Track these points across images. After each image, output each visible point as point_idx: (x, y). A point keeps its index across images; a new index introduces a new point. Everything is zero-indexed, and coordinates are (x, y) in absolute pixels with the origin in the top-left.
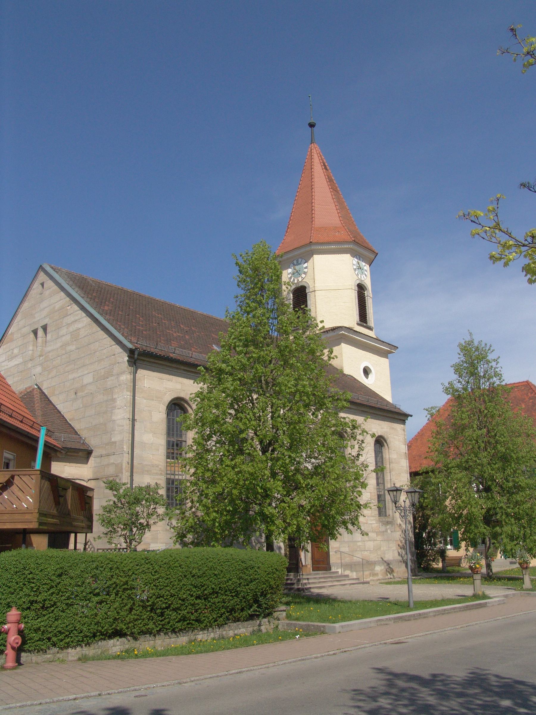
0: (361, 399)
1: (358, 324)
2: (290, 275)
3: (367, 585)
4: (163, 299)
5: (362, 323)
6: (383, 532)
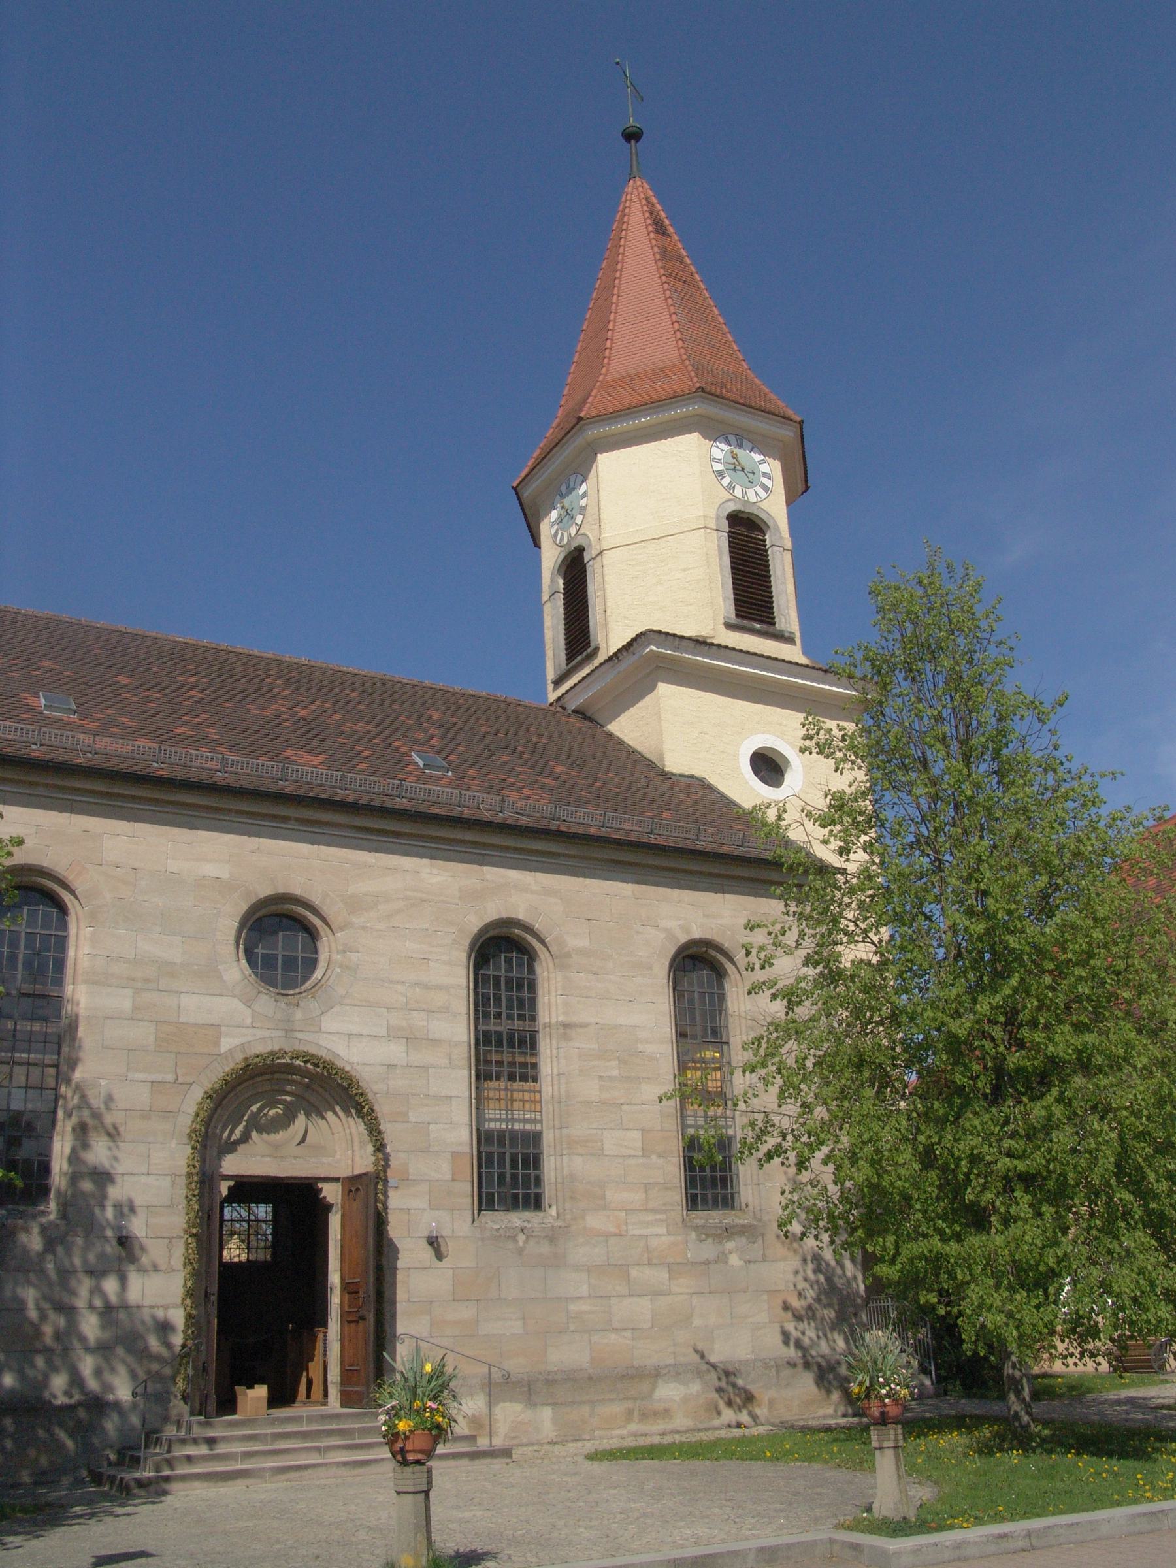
1: (729, 626)
2: (556, 527)
3: (497, 1464)
5: (745, 622)
6: (707, 1263)
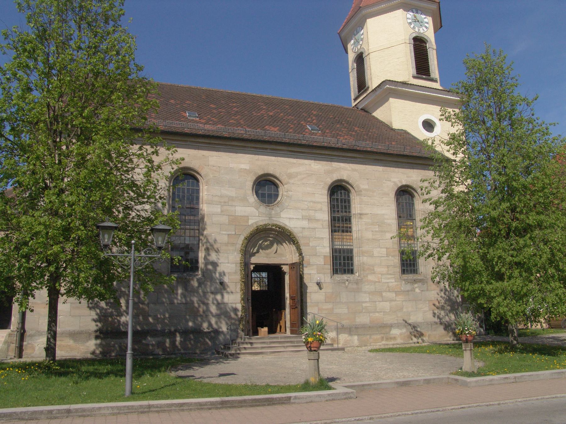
0: (395, 149)
1: (414, 77)
3: (340, 353)
4: (187, 85)
5: (420, 76)
